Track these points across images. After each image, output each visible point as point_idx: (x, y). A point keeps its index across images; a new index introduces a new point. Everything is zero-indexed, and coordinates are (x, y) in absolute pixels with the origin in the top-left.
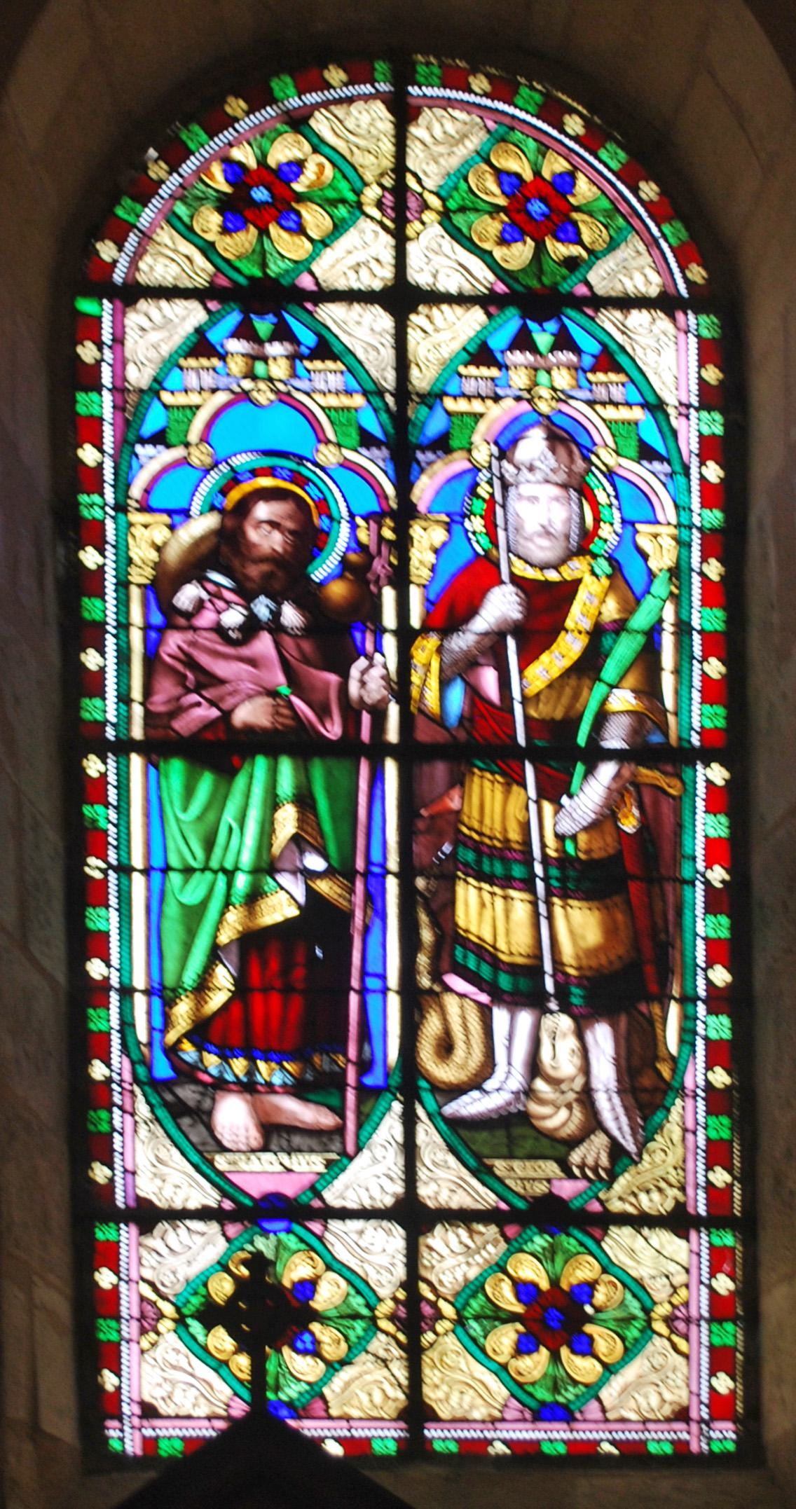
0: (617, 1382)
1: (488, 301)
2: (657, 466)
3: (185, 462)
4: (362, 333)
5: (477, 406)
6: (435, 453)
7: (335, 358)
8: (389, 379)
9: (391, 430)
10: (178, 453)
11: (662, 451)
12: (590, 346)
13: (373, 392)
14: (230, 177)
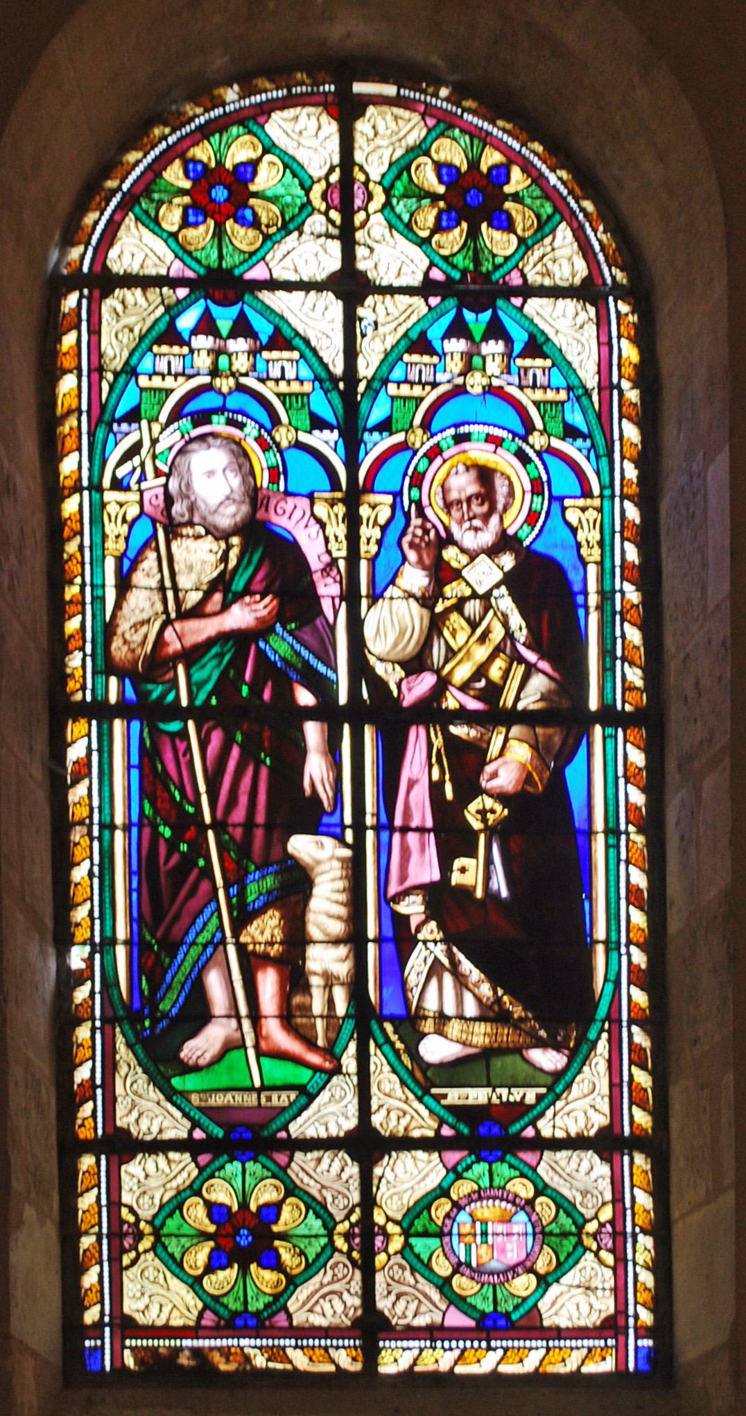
0: (303, 1292)
1: (426, 288)
2: (579, 442)
3: (403, 447)
4: (564, 324)
5: (169, 382)
6: (381, 433)
7: (290, 347)
8: (338, 368)
9: (340, 412)
10: (399, 437)
11: (585, 430)
12: (264, 329)
13: (325, 379)
14: (544, 181)
